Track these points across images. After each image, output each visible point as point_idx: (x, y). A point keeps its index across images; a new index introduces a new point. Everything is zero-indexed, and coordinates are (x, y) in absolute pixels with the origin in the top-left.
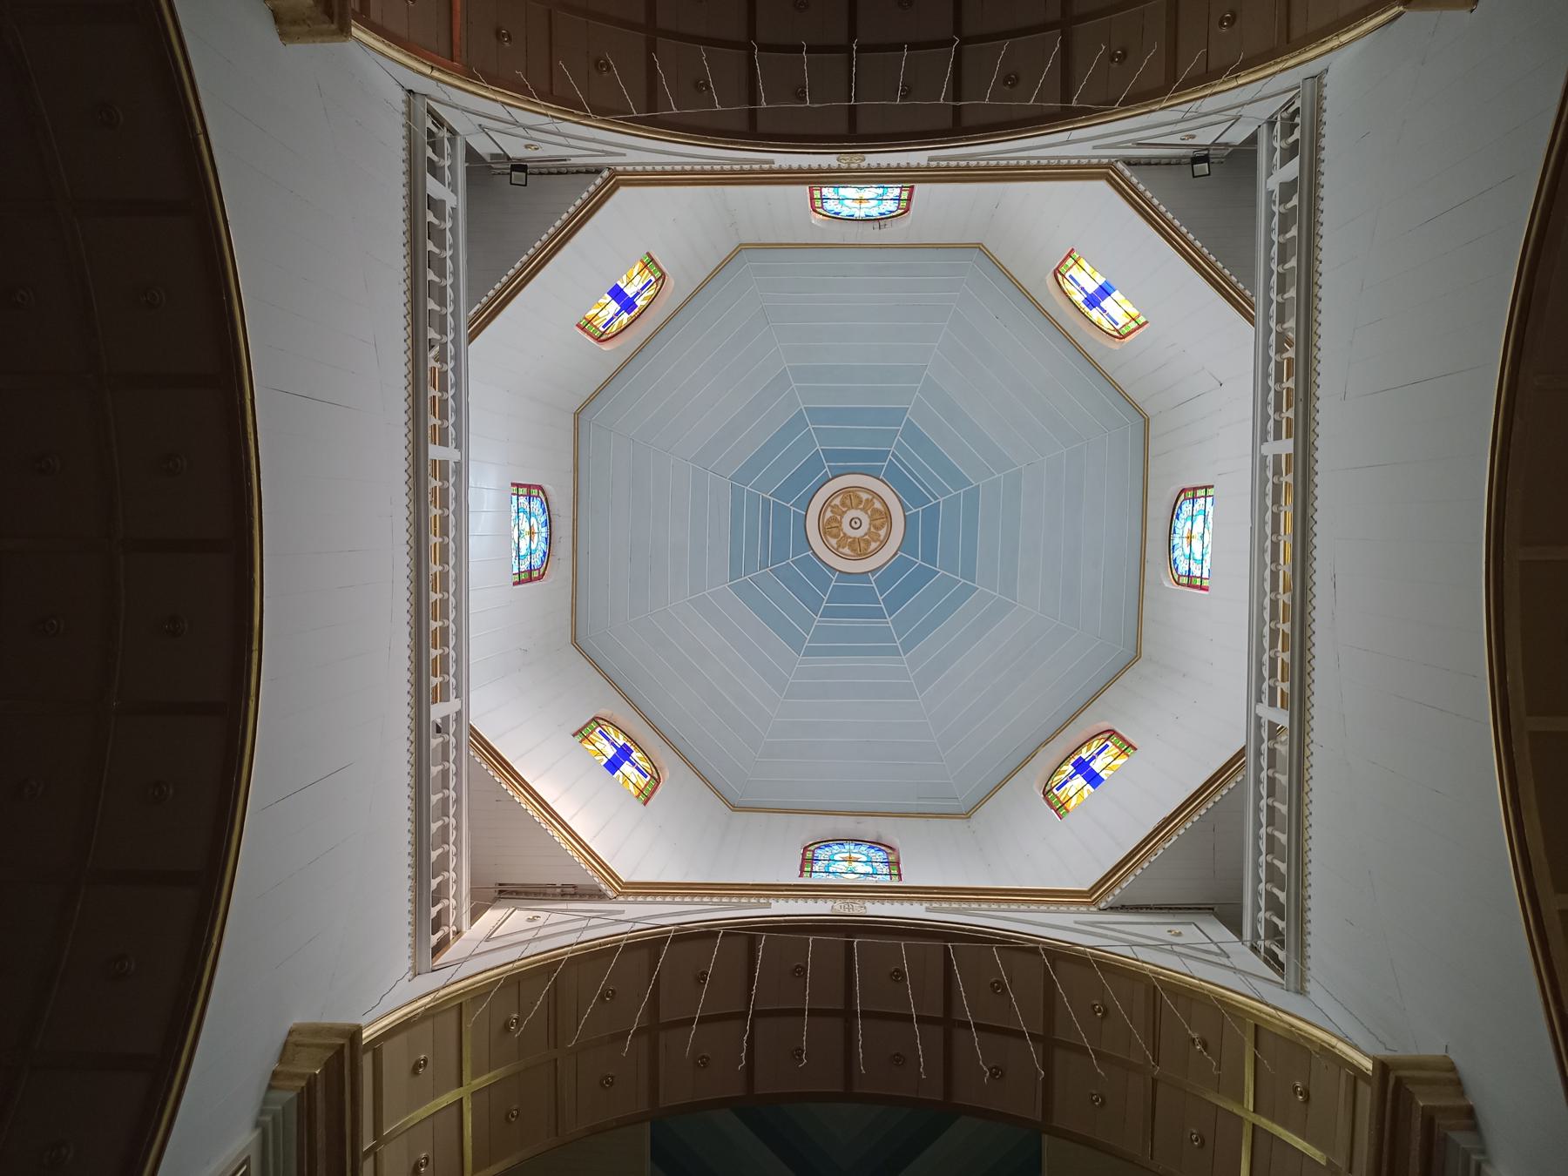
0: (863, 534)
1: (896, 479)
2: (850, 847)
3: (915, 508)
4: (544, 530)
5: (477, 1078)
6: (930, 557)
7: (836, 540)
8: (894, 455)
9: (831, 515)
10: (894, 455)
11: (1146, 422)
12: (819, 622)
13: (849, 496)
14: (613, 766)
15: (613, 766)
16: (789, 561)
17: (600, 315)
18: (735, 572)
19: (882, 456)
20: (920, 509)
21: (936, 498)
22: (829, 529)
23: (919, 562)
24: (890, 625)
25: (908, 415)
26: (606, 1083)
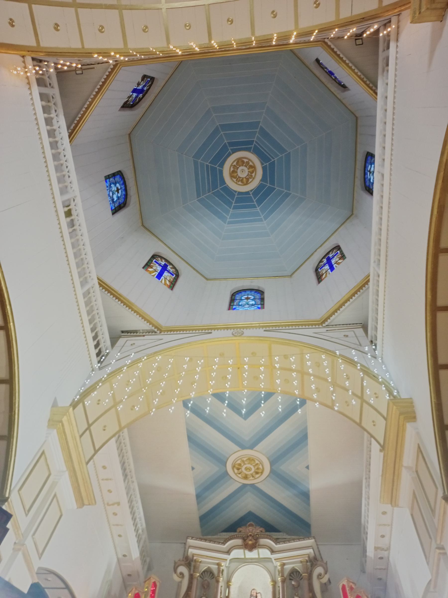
0: (246, 176)
1: (257, 152)
2: (248, 292)
3: (266, 163)
4: (123, 186)
5: (371, 226)
6: (272, 182)
7: (236, 179)
8: (256, 142)
9: (233, 169)
10: (256, 142)
11: (207, 279)
12: (232, 211)
13: (233, 174)
14: (159, 276)
15: (159, 276)
16: (218, 189)
17: (129, 100)
18: (198, 195)
19: (251, 142)
20: (268, 164)
21: (274, 159)
22: (240, 162)
23: (268, 185)
24: (259, 210)
25: (260, 124)
26: (128, 384)
